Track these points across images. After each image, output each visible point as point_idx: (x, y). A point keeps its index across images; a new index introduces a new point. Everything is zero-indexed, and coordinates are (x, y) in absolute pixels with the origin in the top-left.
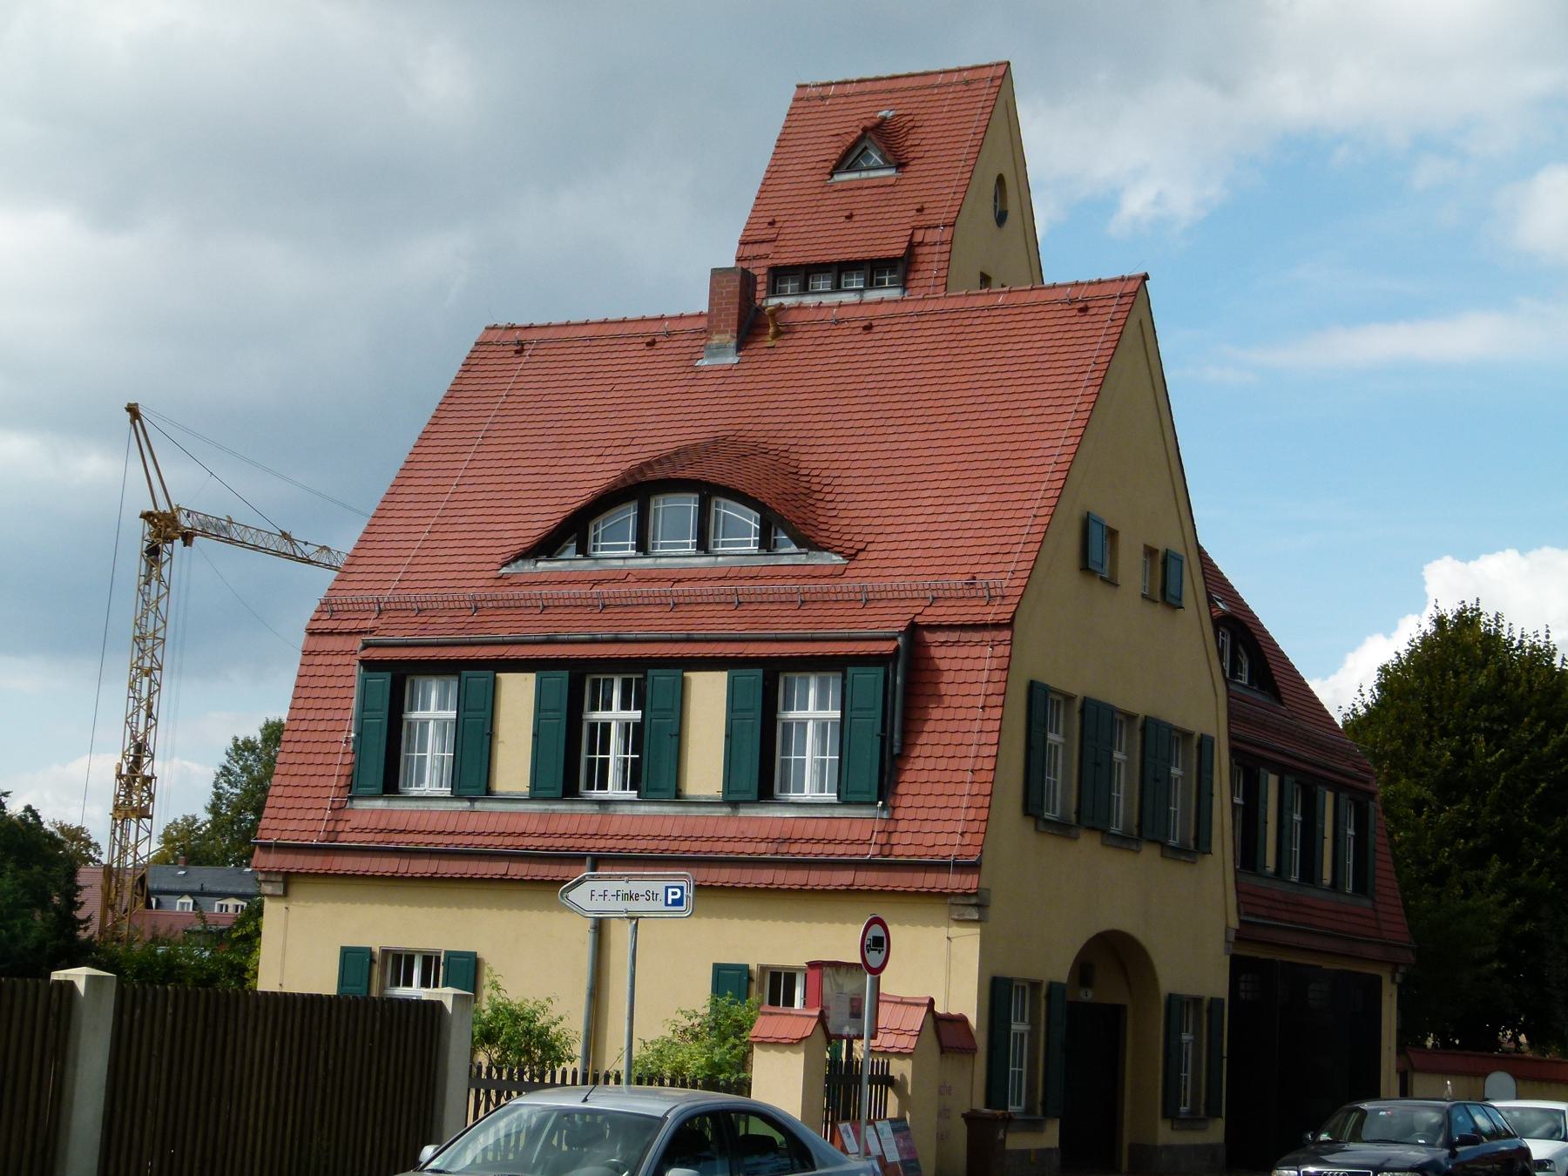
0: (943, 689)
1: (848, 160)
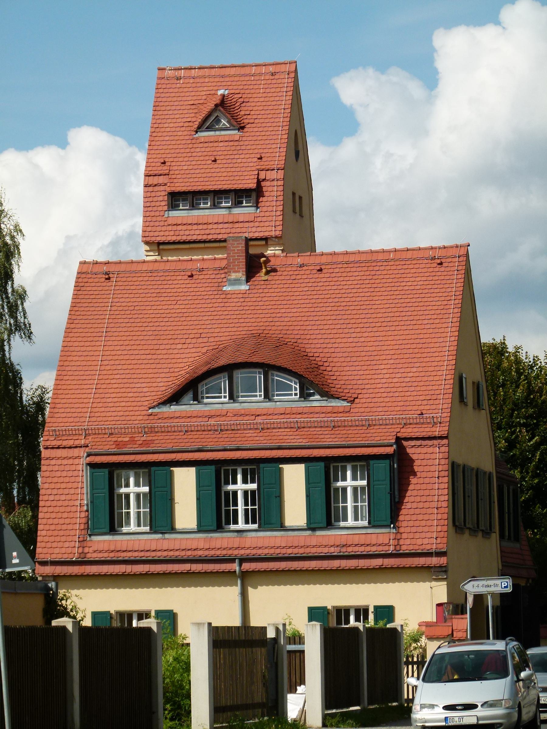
0: (416, 469)
1: (207, 123)
